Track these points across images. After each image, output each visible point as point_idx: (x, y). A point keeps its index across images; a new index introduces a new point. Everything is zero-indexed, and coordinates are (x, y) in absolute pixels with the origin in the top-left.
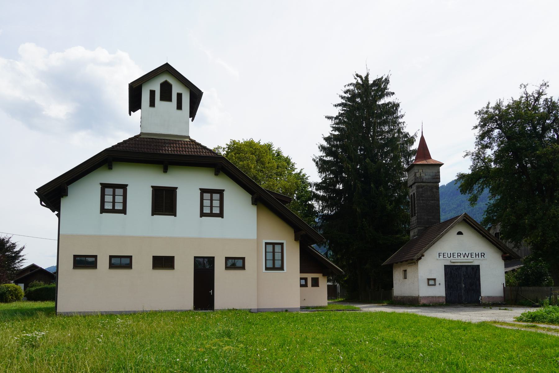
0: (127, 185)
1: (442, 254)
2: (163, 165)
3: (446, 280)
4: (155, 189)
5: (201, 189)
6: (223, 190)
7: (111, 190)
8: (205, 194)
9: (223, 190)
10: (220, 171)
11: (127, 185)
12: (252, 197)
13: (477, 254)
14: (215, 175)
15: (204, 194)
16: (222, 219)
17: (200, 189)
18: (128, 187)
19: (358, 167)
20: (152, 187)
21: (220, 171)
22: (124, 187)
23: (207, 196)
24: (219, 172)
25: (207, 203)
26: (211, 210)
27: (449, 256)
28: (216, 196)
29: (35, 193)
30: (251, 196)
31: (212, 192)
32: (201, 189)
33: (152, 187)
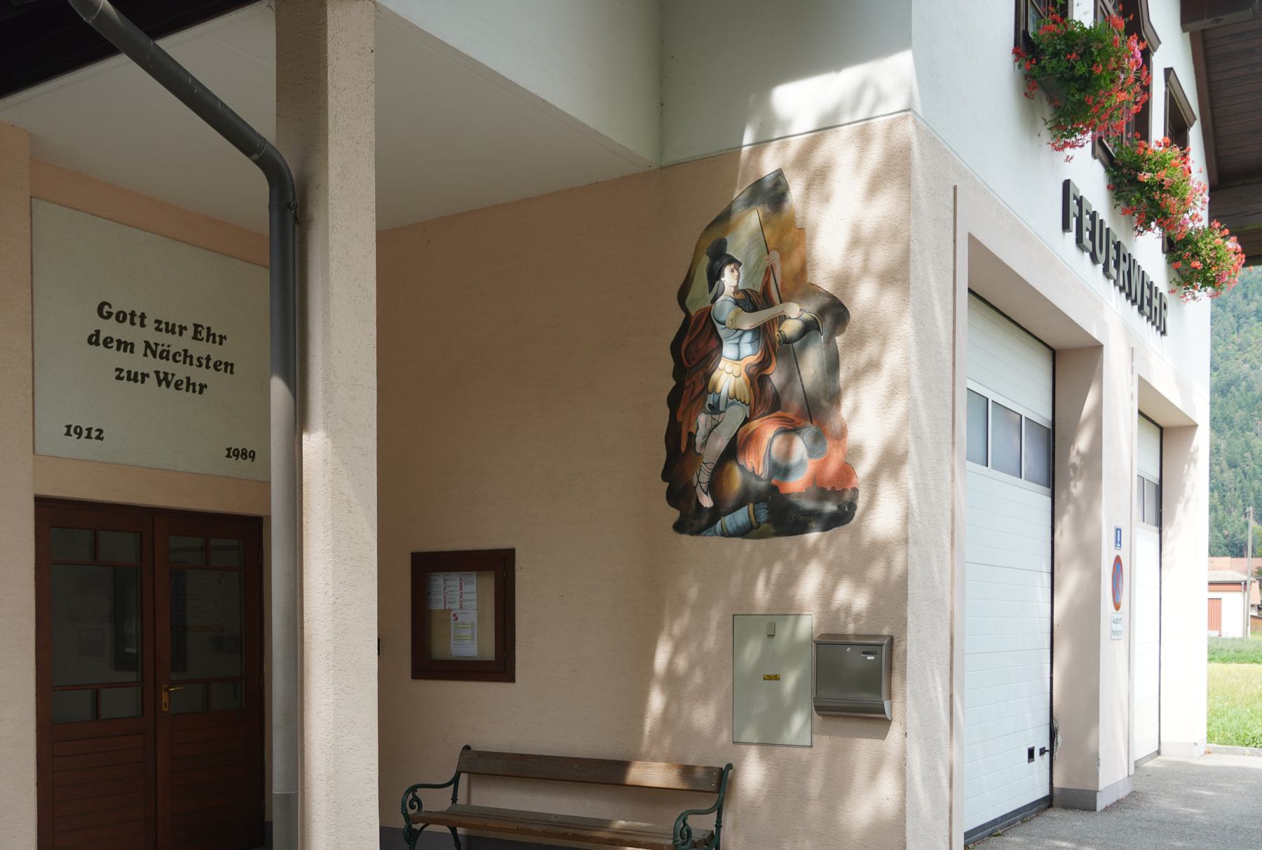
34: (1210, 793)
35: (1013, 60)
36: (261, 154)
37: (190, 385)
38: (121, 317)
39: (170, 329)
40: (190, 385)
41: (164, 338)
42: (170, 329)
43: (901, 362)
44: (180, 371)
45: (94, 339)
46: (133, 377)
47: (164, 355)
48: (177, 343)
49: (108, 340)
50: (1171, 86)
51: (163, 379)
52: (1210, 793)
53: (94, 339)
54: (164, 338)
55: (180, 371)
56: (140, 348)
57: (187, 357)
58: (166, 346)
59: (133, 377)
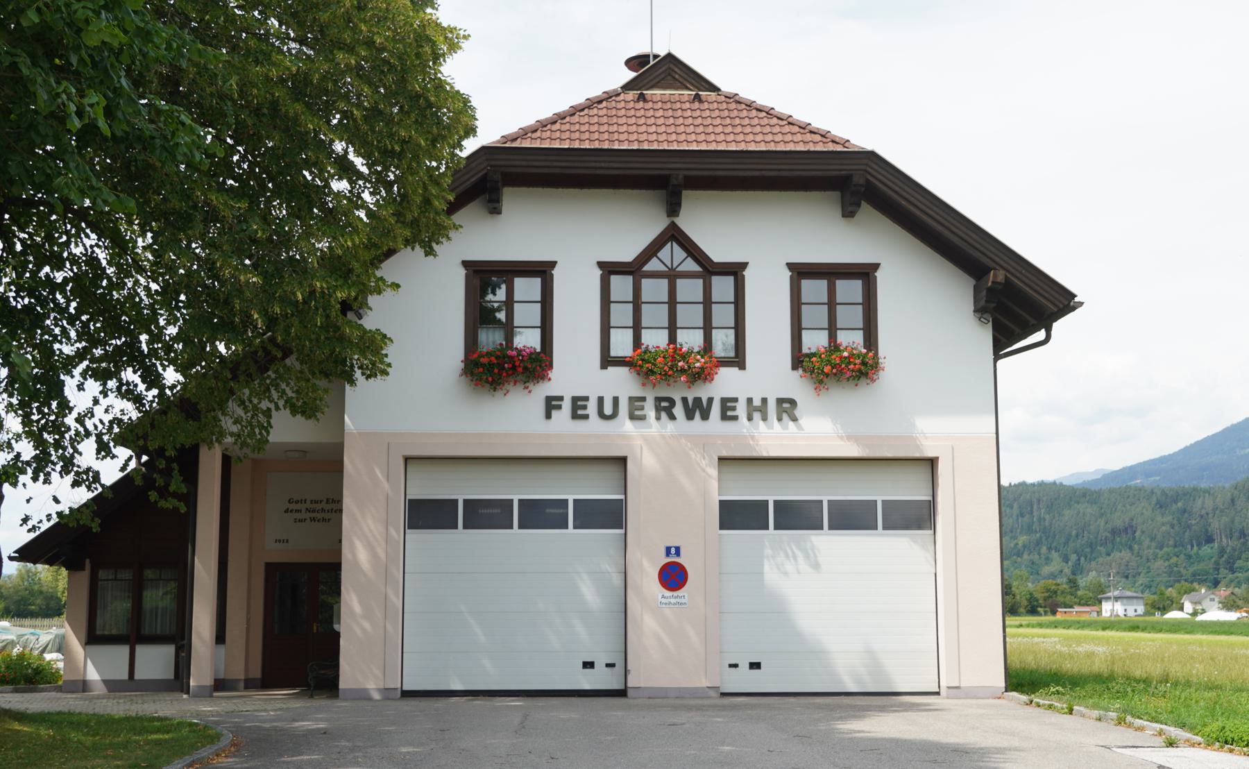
0: (553, 264)
1: (567, 405)
2: (664, 191)
3: (1009, 521)
4: (475, 272)
5: (791, 266)
6: (876, 266)
7: (823, 284)
8: (614, 279)
9: (876, 266)
10: (863, 202)
11: (553, 264)
12: (975, 286)
13: (757, 402)
14: (844, 216)
15: (804, 282)
16: (742, 371)
17: (787, 264)
18: (878, 271)
19: (315, 211)
20: (466, 264)
21: (863, 202)
22: (544, 272)
23: (814, 289)
24: (859, 205)
25: (815, 315)
26: (672, 339)
27: (608, 410)
28: (850, 290)
29: (371, 309)
30: (972, 282)
31: (831, 273)
32: (791, 266)
33: (466, 264)
34: (411, 749)
35: (813, 389)
36: (73, 114)
37: (324, 520)
38: (297, 502)
39: (316, 502)
40: (324, 520)
41: (314, 506)
42: (316, 502)
43: (789, 567)
44: (320, 516)
45: (286, 511)
46: (301, 521)
47: (314, 511)
48: (318, 507)
49: (291, 511)
50: (713, 706)
51: (313, 520)
52: (411, 749)
53: (286, 511)
54: (314, 506)
55: (320, 516)
56: (304, 511)
57: (323, 510)
58: (308, 502)
59: (301, 521)
